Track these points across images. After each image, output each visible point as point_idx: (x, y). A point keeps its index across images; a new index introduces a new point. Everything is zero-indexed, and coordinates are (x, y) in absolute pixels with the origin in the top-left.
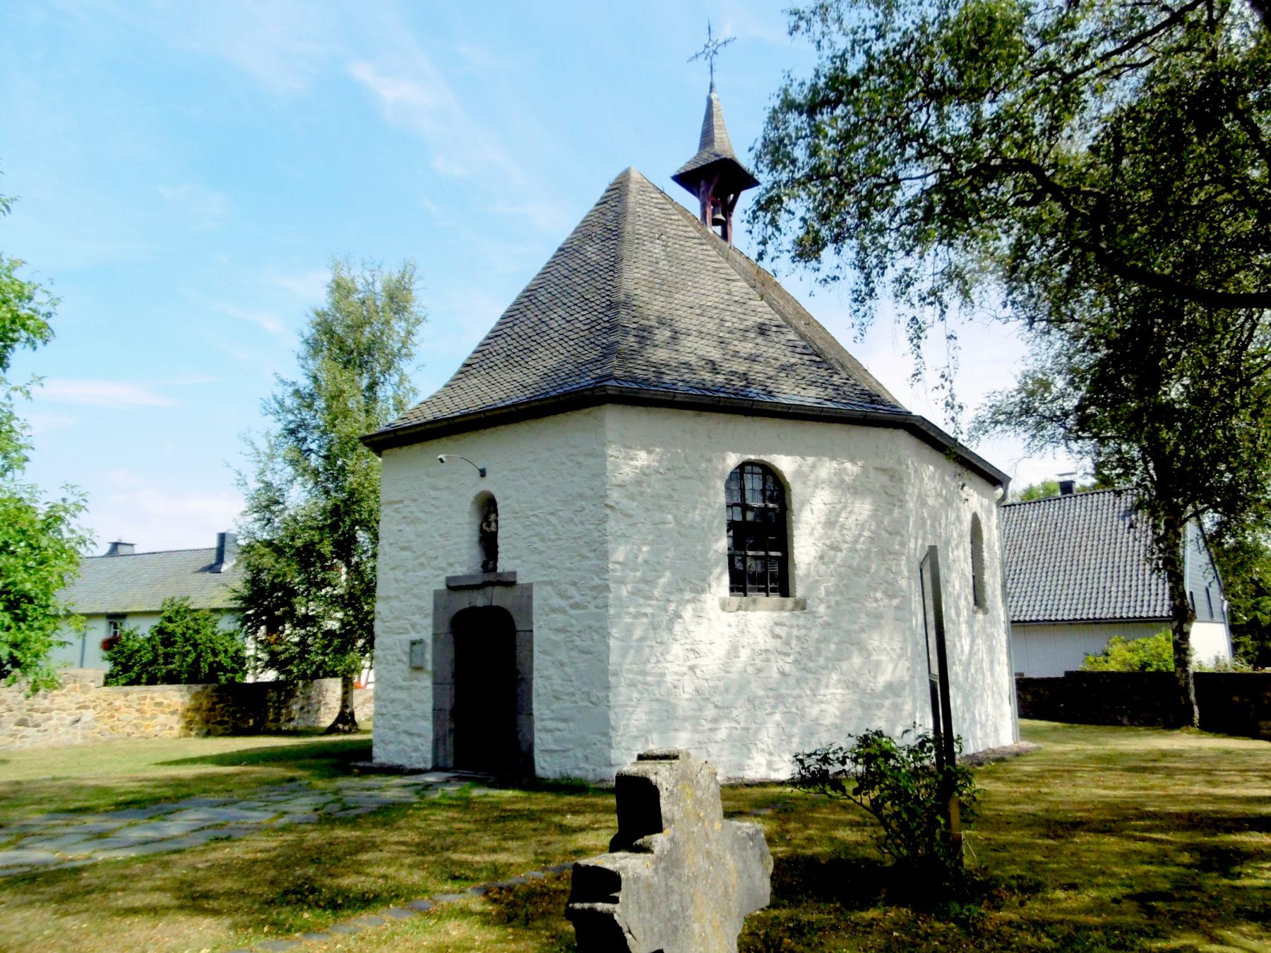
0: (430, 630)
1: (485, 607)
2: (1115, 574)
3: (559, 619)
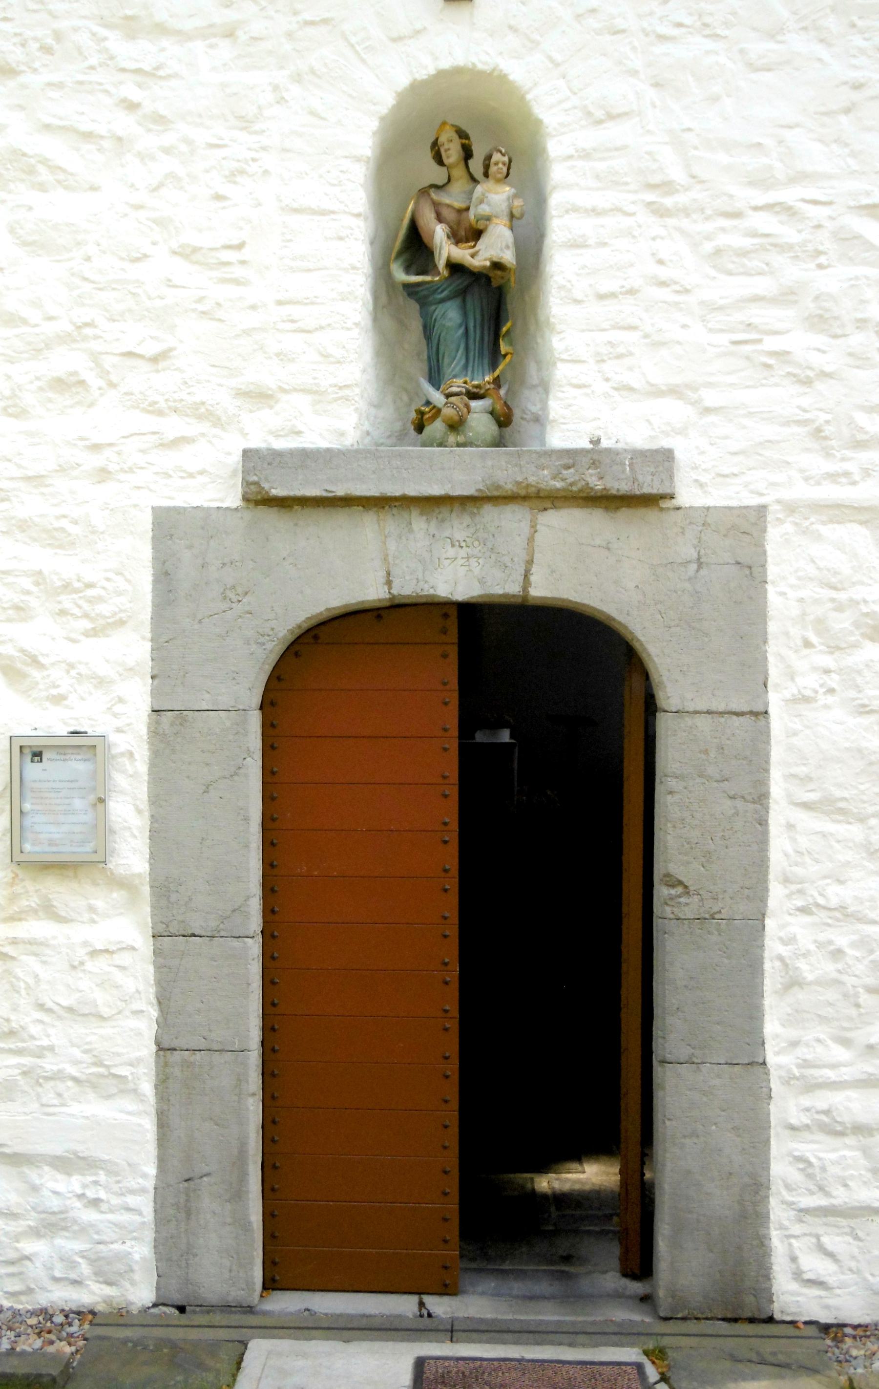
0: (138, 697)
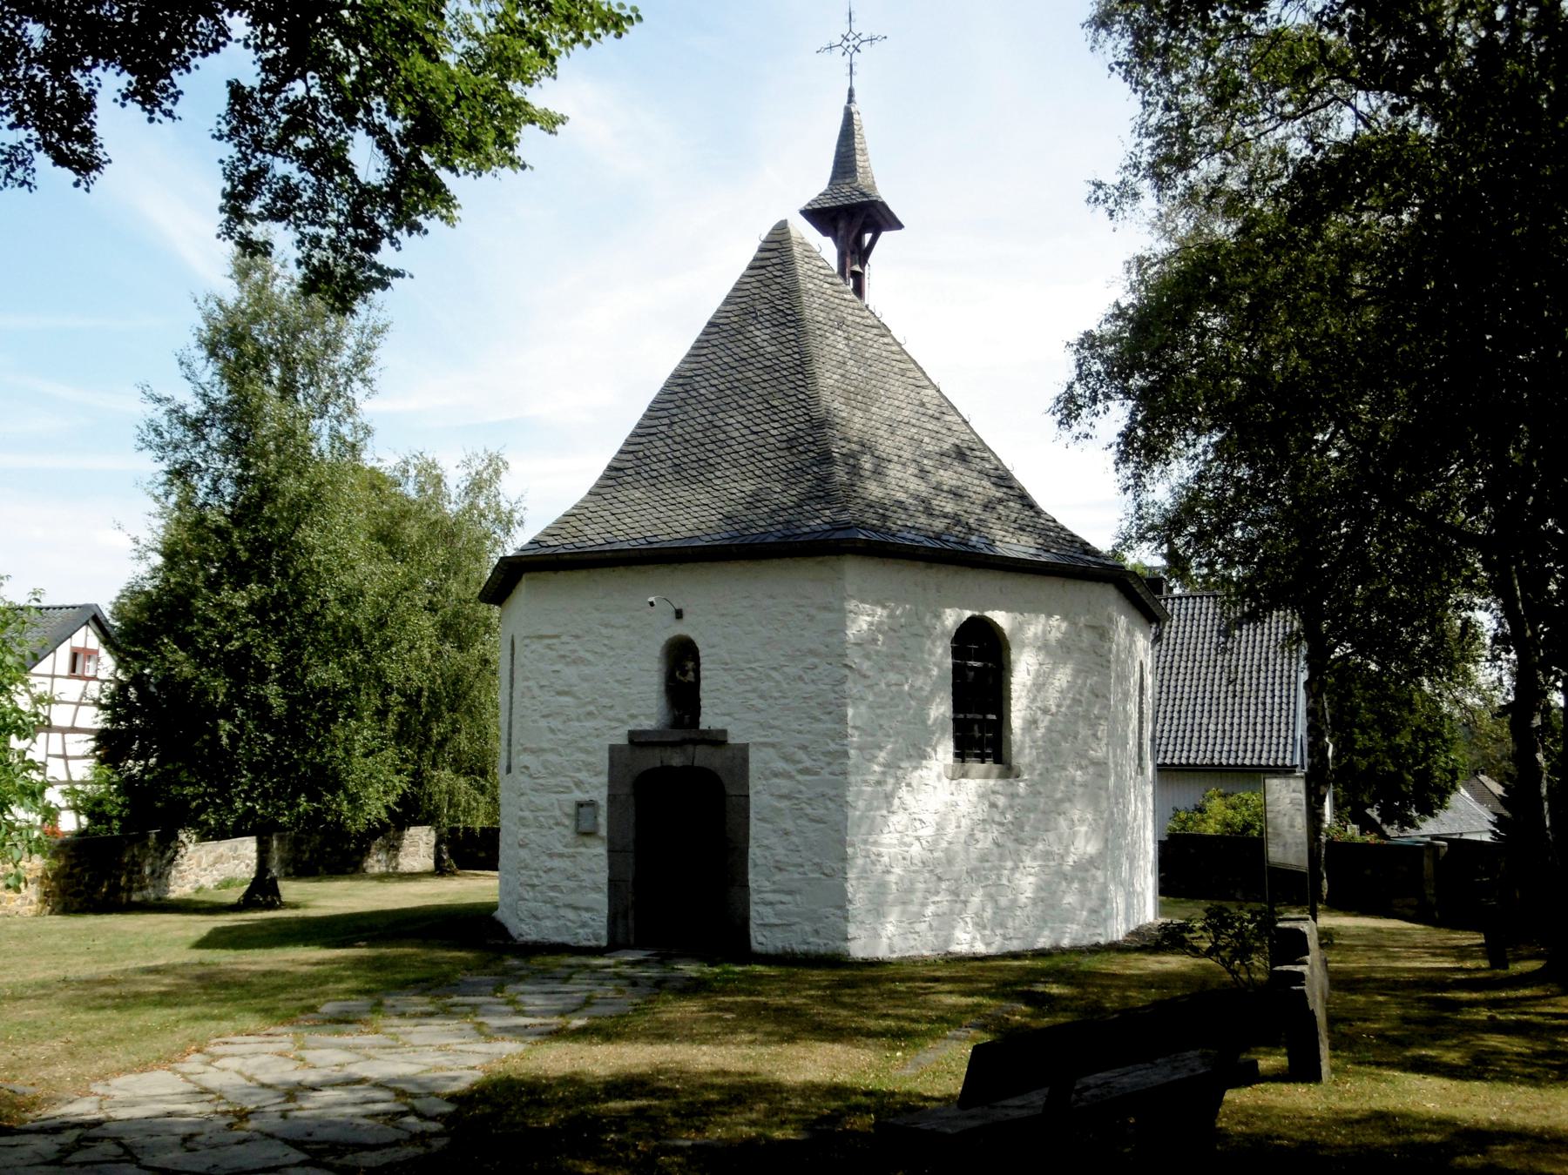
0: (605, 792)
1: (684, 768)
2: (1214, 708)
3: (784, 785)
